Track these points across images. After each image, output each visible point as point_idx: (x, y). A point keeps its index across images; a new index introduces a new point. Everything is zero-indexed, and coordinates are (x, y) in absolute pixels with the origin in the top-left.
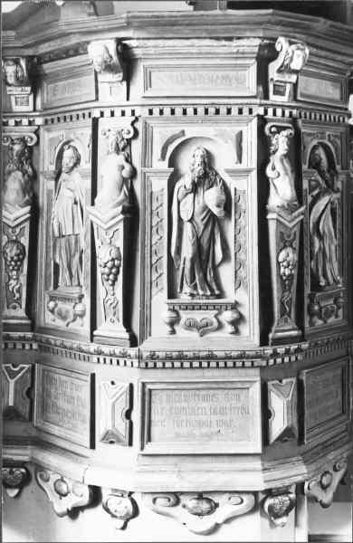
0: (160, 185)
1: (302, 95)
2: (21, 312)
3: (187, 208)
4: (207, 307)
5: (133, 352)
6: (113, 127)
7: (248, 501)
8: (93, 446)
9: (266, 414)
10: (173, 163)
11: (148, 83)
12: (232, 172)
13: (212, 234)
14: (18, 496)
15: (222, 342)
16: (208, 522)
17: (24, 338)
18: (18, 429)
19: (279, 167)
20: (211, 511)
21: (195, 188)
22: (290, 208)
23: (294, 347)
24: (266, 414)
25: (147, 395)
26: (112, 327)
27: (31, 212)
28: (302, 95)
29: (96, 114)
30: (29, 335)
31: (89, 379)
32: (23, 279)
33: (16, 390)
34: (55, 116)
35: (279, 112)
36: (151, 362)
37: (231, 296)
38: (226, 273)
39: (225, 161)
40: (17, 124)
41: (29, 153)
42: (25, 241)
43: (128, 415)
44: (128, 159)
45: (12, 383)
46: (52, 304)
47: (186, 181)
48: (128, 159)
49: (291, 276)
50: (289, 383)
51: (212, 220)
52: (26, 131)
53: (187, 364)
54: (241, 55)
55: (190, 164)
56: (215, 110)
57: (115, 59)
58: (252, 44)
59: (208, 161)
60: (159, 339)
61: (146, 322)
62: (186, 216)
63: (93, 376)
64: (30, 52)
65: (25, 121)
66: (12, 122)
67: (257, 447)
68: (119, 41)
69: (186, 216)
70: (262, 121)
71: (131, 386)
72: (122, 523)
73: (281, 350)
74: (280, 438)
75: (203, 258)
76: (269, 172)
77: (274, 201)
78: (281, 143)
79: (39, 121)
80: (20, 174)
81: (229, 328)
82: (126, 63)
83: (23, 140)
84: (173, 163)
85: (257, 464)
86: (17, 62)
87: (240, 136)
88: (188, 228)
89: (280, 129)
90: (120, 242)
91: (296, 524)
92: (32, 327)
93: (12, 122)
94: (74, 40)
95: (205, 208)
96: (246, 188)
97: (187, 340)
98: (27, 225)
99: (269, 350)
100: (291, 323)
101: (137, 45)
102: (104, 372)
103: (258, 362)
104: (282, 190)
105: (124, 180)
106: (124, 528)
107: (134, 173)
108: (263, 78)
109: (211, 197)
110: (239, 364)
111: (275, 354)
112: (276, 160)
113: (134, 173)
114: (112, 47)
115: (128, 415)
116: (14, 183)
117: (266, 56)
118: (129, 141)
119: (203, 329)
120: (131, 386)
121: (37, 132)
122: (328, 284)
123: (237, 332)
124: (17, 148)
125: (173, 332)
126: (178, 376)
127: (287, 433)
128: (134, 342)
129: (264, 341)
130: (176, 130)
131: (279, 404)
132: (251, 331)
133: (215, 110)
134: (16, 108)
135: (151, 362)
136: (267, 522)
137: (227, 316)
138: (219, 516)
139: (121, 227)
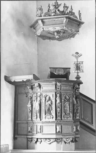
0: (44, 101)
1: (62, 89)
2: (31, 119)
3: (47, 103)
4: (49, 116)
5: (40, 121)
6: (39, 94)
7: (54, 140)
8: (37, 134)
9: (56, 129)
10: (45, 98)
11: (42, 89)
12: (52, 99)
13: (50, 107)
14: (31, 142)
15: (51, 120)
16: (49, 142)
17: (31, 122)
18: (30, 134)
19: (58, 98)
20: (50, 141)
21: (48, 101)
22: (59, 103)
23: (60, 121)
24: (56, 129)
25: (42, 127)
26: (39, 119)
27: (31, 105)
28: (62, 89)
29: (37, 92)
30: (31, 121)
31: (36, 125)
32: (31, 114)
33: (63, 147)
34: (34, 93)
35: (58, 91)
36: (43, 123)
37: (52, 114)
38: (52, 111)
39: (51, 98)
40: (30, 94)
41: (32, 98)
42: (31, 109)
43: (40, 129)
44: (40, 98)
45: (29, 128)
46: (34, 117)
47: (47, 100)
48: (40, 98)
49: (59, 112)
50: (60, 126)
51: (50, 105)
52: (31, 95)
53: (47, 123)
54: (53, 84)
55: (47, 98)
56: (50, 91)
57: (38, 86)
58: (54, 83)
59: (50, 98)
60: (44, 120)
61: (42, 118)
62: (47, 105)
63: (37, 125)
64: (31, 85)
65: (31, 94)
66: (29, 94)
67: (55, 133)
68: (38, 83)
69: (47, 105)
70: (56, 93)
71: (41, 126)
72: (40, 143)
73: (58, 121)
74: (58, 132)
75: (49, 110)
76: (57, 99)
77: (57, 102)
78: (58, 95)
79: (33, 94)
80: (30, 101)
81: (52, 118)
82: (40, 86)
83: (31, 96)
84: (45, 98)
85: (55, 135)
86: (29, 86)
87: (53, 94)
88: (47, 106)
89: (58, 93)
90: (39, 108)
91: (61, 144)
92: (32, 121)
93: (29, 94)
94: (34, 83)
95: (49, 104)
96: (54, 101)
97: (47, 120)
98: (31, 107)
99: (56, 121)
100: (60, 118)
101: (41, 84)
102: (38, 124)
103: (55, 122)
104: (58, 101)
105: (40, 101)
106: (40, 143)
107: (41, 100)
108: (56, 87)
109: (49, 102)
110: (52, 123)
111: (57, 122)
112: (57, 97)
113: (41, 100)
114: (37, 84)
115: (40, 129)
116: (30, 102)
117: (56, 85)
118: (40, 96)
119: (49, 118)
120: (41, 126)
121: (32, 95)
122: (67, 114)
123: (53, 119)
124: (30, 97)
125: (45, 119)
126: (46, 124)
127: (59, 131)
128: (41, 120)
129: (56, 120)
130: (46, 94)
131: (58, 127)
132: (54, 118)
133: (50, 91)
134: (30, 92)
135: (43, 123)
136: (57, 143)
137: (52, 117)
138: (51, 142)
139: (39, 106)
